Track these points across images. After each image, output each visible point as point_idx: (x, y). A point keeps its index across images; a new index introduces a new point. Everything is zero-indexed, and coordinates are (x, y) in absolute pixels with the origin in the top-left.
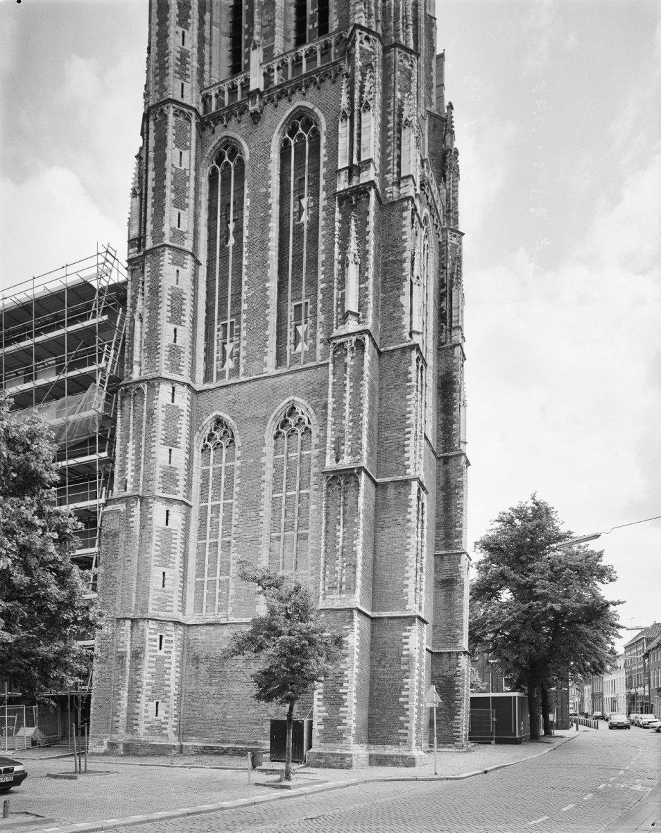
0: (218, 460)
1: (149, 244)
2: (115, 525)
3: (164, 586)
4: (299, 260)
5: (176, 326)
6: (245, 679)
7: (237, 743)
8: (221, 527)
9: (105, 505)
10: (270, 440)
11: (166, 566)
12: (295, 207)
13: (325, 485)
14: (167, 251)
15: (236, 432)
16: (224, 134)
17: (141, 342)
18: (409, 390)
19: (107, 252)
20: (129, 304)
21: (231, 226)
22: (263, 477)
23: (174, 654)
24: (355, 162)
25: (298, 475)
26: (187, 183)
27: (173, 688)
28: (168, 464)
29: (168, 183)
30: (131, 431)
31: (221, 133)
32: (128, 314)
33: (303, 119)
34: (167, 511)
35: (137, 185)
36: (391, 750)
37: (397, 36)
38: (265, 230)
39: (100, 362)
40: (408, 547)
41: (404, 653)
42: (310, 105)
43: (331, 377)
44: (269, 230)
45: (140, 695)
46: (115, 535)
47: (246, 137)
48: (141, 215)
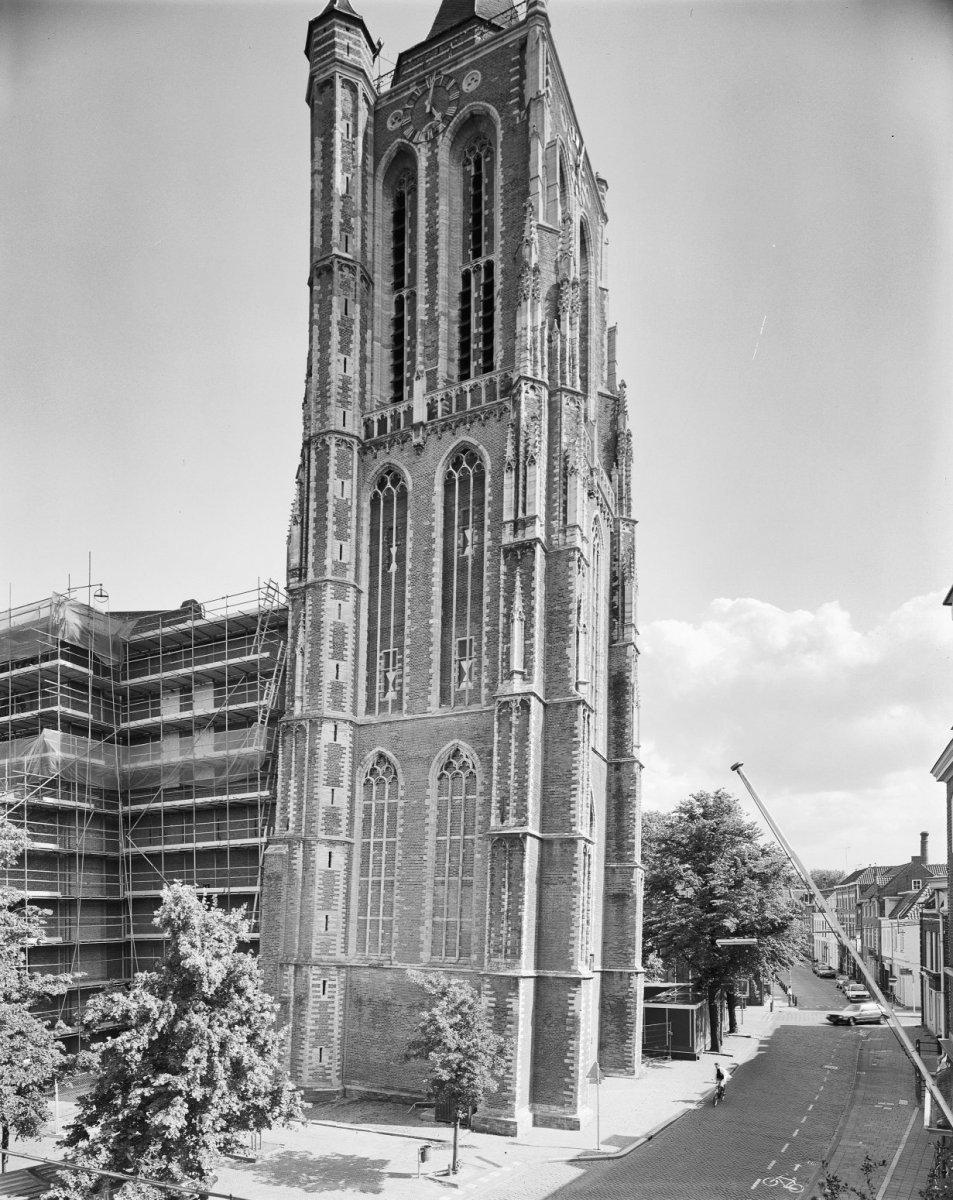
0: (381, 796)
1: (311, 577)
2: (277, 867)
3: (326, 929)
4: (463, 593)
5: (338, 662)
6: (409, 1027)
7: (402, 1090)
8: (384, 866)
9: (267, 844)
10: (433, 782)
11: (329, 909)
12: (459, 539)
13: (489, 848)
14: (330, 586)
15: (399, 771)
16: (386, 461)
17: (303, 676)
18: (575, 746)
19: (269, 587)
20: (289, 636)
21: (394, 550)
22: (427, 820)
23: (337, 997)
24: (521, 515)
25: (462, 820)
26: (349, 513)
27: (336, 1033)
28: (330, 804)
29: (330, 515)
30: (293, 769)
31: (382, 459)
32: (289, 646)
33: (465, 455)
34: (330, 853)
35: (298, 513)
36: (555, 1110)
37: (563, 378)
38: (429, 564)
39: (261, 699)
40: (574, 906)
41: (570, 1014)
42: (475, 443)
43: (496, 735)
44: (433, 565)
45: (303, 1042)
46: (279, 878)
47: (409, 466)
48: (302, 543)
